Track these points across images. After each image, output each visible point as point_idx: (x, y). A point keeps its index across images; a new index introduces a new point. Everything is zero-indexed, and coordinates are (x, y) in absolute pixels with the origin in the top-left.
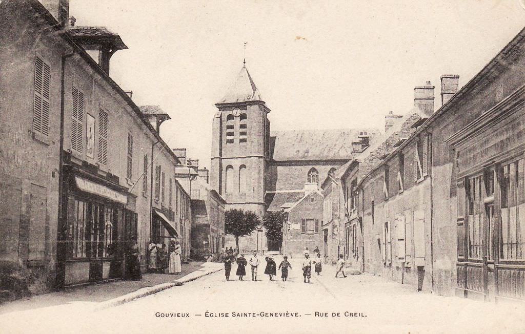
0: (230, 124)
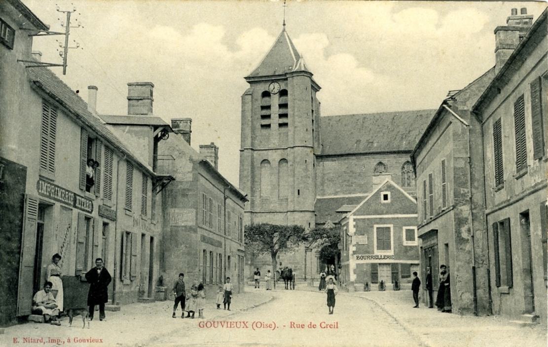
0: (265, 104)
